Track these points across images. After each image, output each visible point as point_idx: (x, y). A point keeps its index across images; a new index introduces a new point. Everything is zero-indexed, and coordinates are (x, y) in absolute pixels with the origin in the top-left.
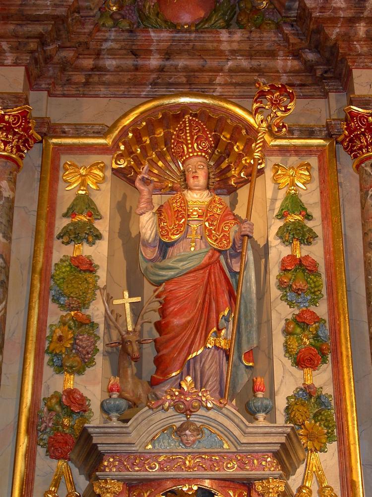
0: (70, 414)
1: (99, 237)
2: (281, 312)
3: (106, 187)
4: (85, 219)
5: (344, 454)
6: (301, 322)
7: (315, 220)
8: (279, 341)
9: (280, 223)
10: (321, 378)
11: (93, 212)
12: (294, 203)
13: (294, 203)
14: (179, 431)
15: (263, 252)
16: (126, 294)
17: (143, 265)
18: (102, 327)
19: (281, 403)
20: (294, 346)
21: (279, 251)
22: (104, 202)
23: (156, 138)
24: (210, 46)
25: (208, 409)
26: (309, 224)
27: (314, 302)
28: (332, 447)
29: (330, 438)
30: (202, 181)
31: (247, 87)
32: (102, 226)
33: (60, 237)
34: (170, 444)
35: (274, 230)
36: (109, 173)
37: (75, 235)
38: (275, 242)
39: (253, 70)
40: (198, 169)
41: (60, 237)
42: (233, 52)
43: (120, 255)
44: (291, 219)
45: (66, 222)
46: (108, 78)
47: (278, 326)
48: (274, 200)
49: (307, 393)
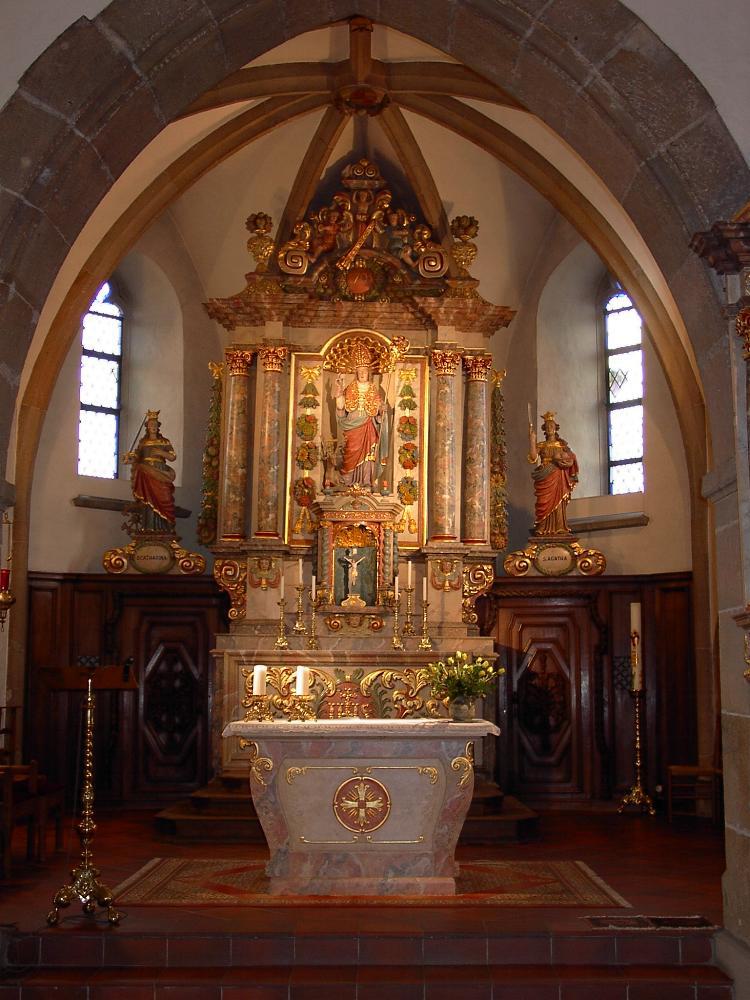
0: (307, 487)
1: (318, 405)
2: (399, 442)
3: (321, 378)
4: (311, 396)
5: (420, 507)
6: (406, 448)
7: (452, 204)
8: (397, 456)
9: (401, 399)
10: (412, 474)
11: (316, 393)
12: (408, 390)
13: (408, 390)
14: (353, 504)
15: (392, 412)
16: (349, 741)
17: (337, 419)
18: (320, 448)
19: (396, 484)
20: (403, 460)
21: (400, 413)
22: (320, 387)
23: (343, 354)
24: (371, 309)
25: (356, 547)
26: (414, 399)
27: (414, 438)
28: (416, 503)
29: (415, 499)
30: (365, 379)
31: (387, 327)
32: (319, 399)
33: (300, 404)
34: (350, 508)
35: (398, 403)
36: (322, 371)
37: (306, 404)
38: (398, 409)
40: (364, 372)
41: (300, 404)
43: (327, 409)
44: (406, 398)
45: (303, 396)
46: (321, 320)
47: (397, 449)
48: (398, 387)
49: (407, 480)
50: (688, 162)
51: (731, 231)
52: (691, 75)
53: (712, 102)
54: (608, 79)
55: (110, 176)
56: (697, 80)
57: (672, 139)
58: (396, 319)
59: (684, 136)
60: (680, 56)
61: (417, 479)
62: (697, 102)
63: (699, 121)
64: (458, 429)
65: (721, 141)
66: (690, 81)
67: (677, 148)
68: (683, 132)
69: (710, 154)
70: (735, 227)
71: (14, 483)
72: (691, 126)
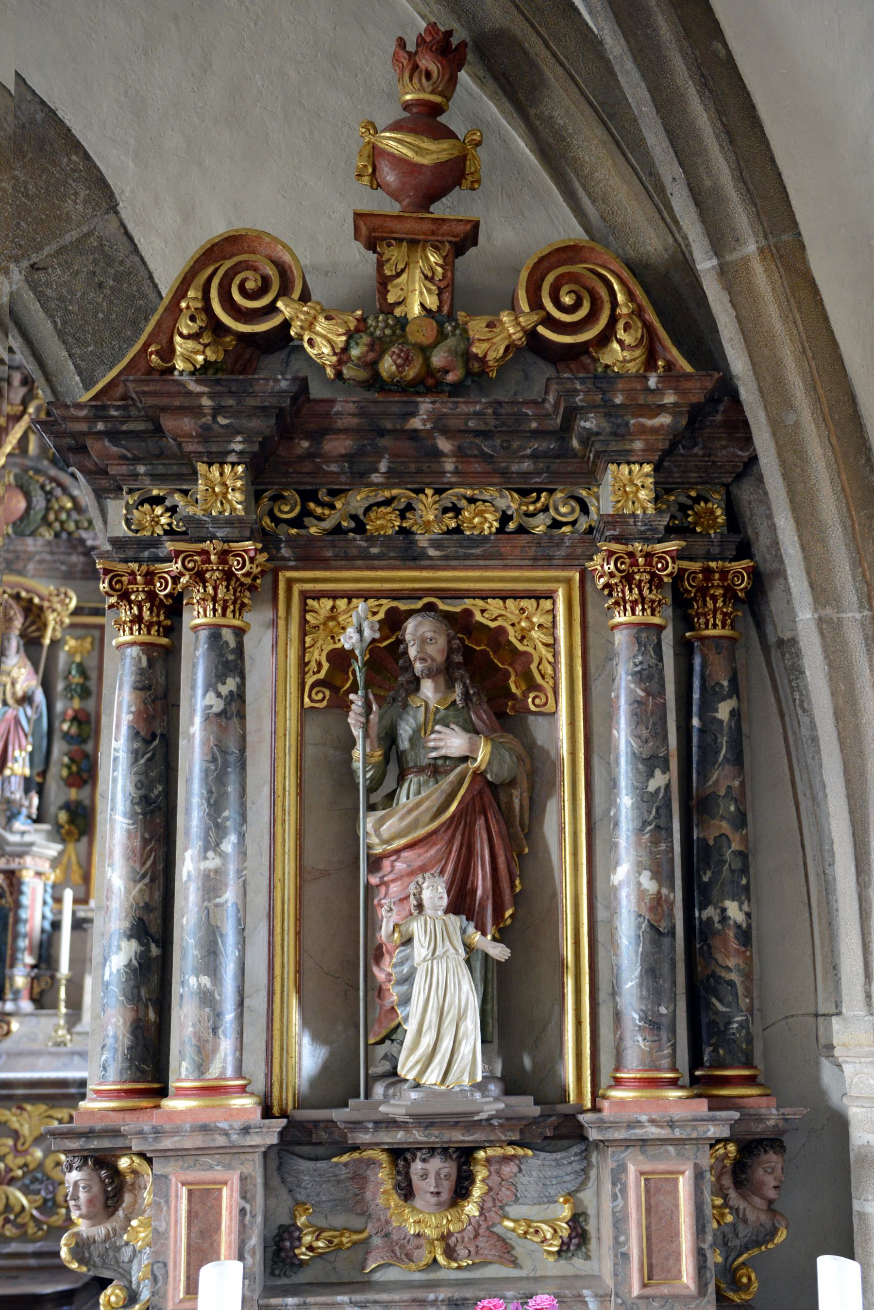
28: (85, 840)
29: (82, 833)
39: (54, 561)
42: (40, 553)
50: (61, 299)
51: (77, 419)
52: (76, 146)
53: (111, 196)
54: (41, 249)
55: (248, 1293)
56: (87, 157)
57: (34, 258)
58: (62, 563)
59: (60, 251)
60: (60, 113)
61: (87, 802)
62: (83, 194)
63: (85, 229)
64: (446, 1023)
65: (122, 262)
66: (74, 158)
67: (42, 274)
68: (54, 246)
69: (100, 285)
70: (83, 413)
71: (438, 119)
72: (68, 238)
